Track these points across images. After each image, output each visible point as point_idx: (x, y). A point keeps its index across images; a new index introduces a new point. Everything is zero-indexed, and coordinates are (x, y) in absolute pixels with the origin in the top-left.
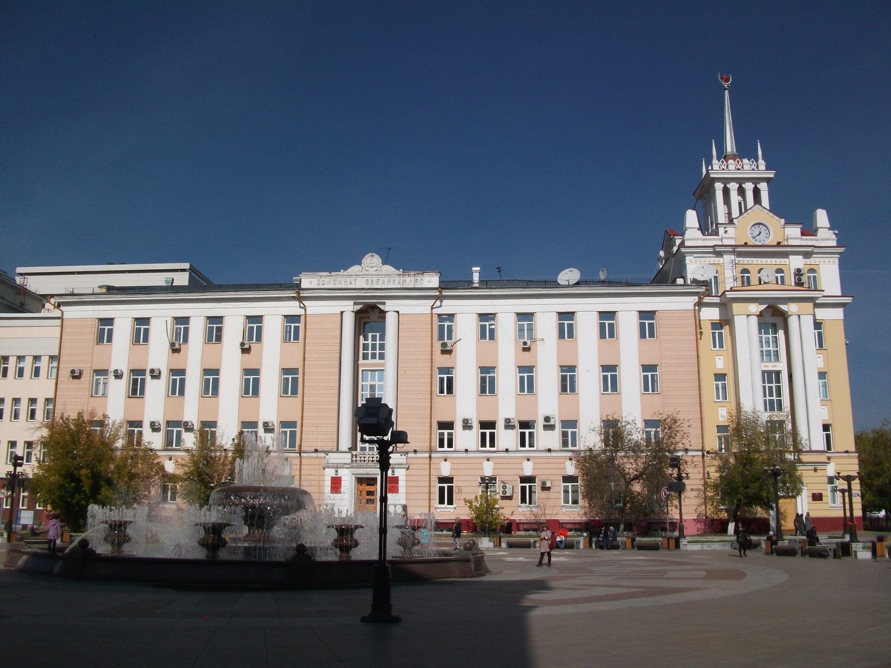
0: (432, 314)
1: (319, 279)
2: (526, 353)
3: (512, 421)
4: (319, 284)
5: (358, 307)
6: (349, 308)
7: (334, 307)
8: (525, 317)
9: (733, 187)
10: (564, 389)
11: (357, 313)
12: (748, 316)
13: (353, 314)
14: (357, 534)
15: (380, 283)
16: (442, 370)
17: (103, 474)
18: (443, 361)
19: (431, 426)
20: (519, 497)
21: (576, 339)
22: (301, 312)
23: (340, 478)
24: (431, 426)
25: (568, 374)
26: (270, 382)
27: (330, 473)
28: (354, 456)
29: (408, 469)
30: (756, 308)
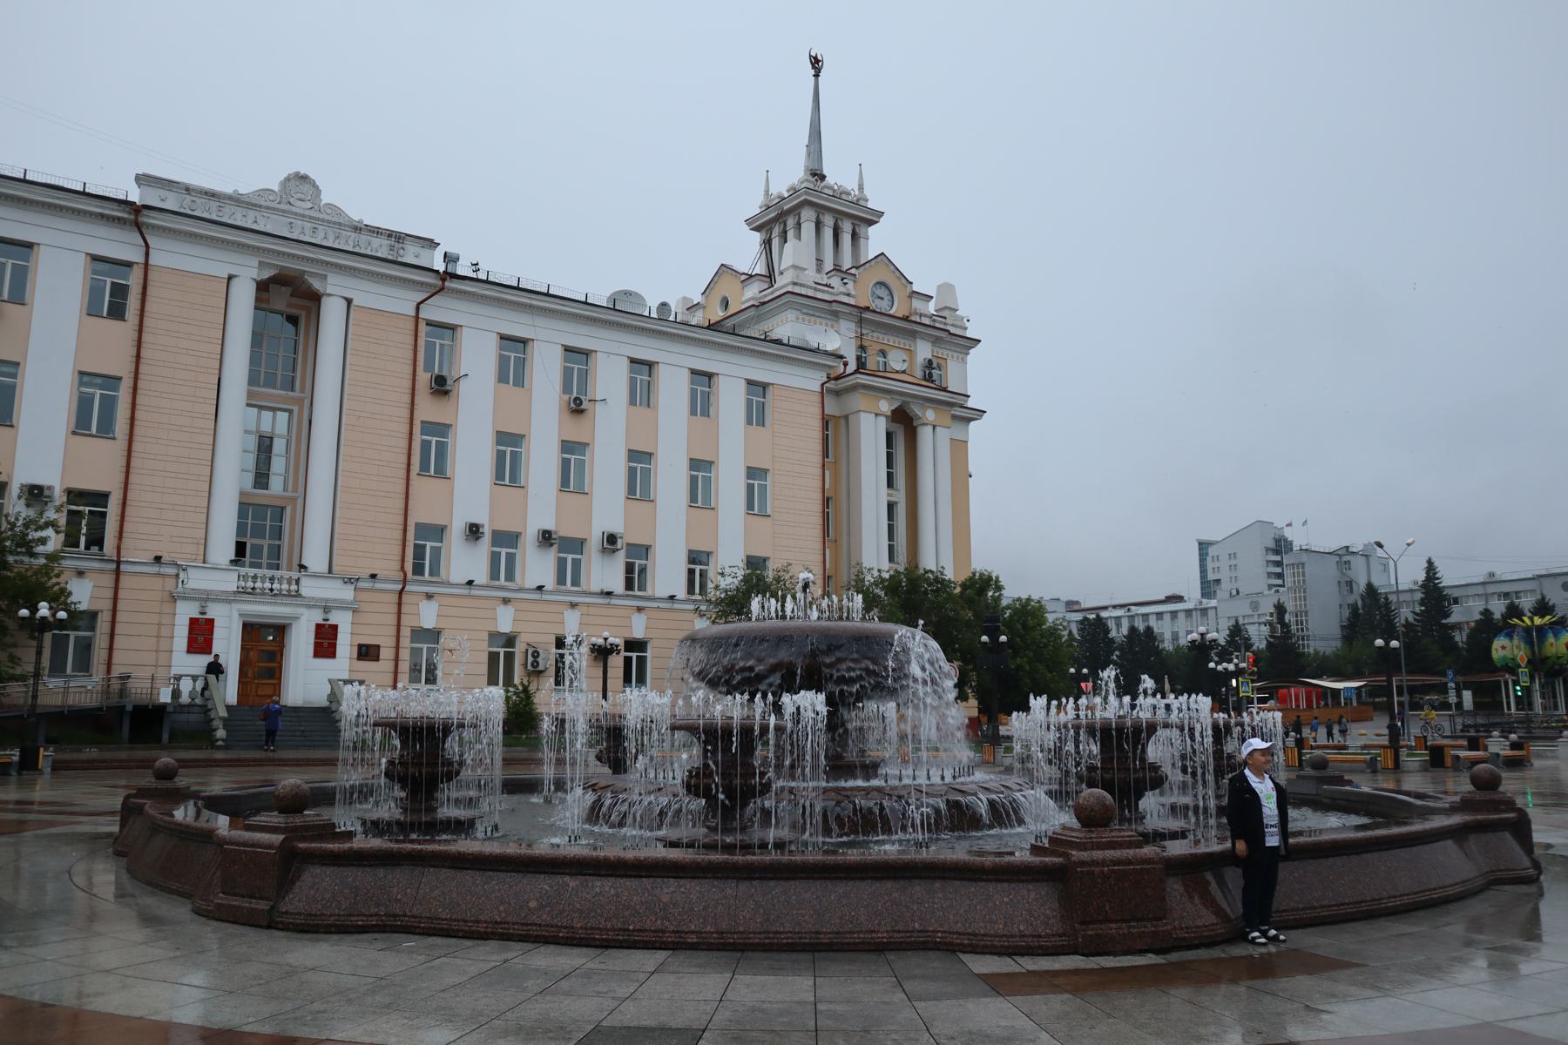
0: (417, 317)
1: (731, 311)
2: (1383, 543)
3: (554, 536)
4: (182, 207)
5: (267, 274)
6: (248, 274)
7: (216, 264)
8: (703, 377)
9: (847, 227)
10: (499, 475)
11: (262, 287)
12: (877, 415)
13: (254, 286)
14: (452, 746)
15: (369, 249)
16: (429, 427)
17: (807, 661)
18: (429, 410)
19: (405, 531)
20: (652, 673)
21: (656, 408)
22: (136, 256)
23: (211, 622)
24: (405, 531)
25: (509, 449)
26: (730, 485)
27: (186, 612)
28: (294, 582)
29: (355, 611)
30: (886, 406)
